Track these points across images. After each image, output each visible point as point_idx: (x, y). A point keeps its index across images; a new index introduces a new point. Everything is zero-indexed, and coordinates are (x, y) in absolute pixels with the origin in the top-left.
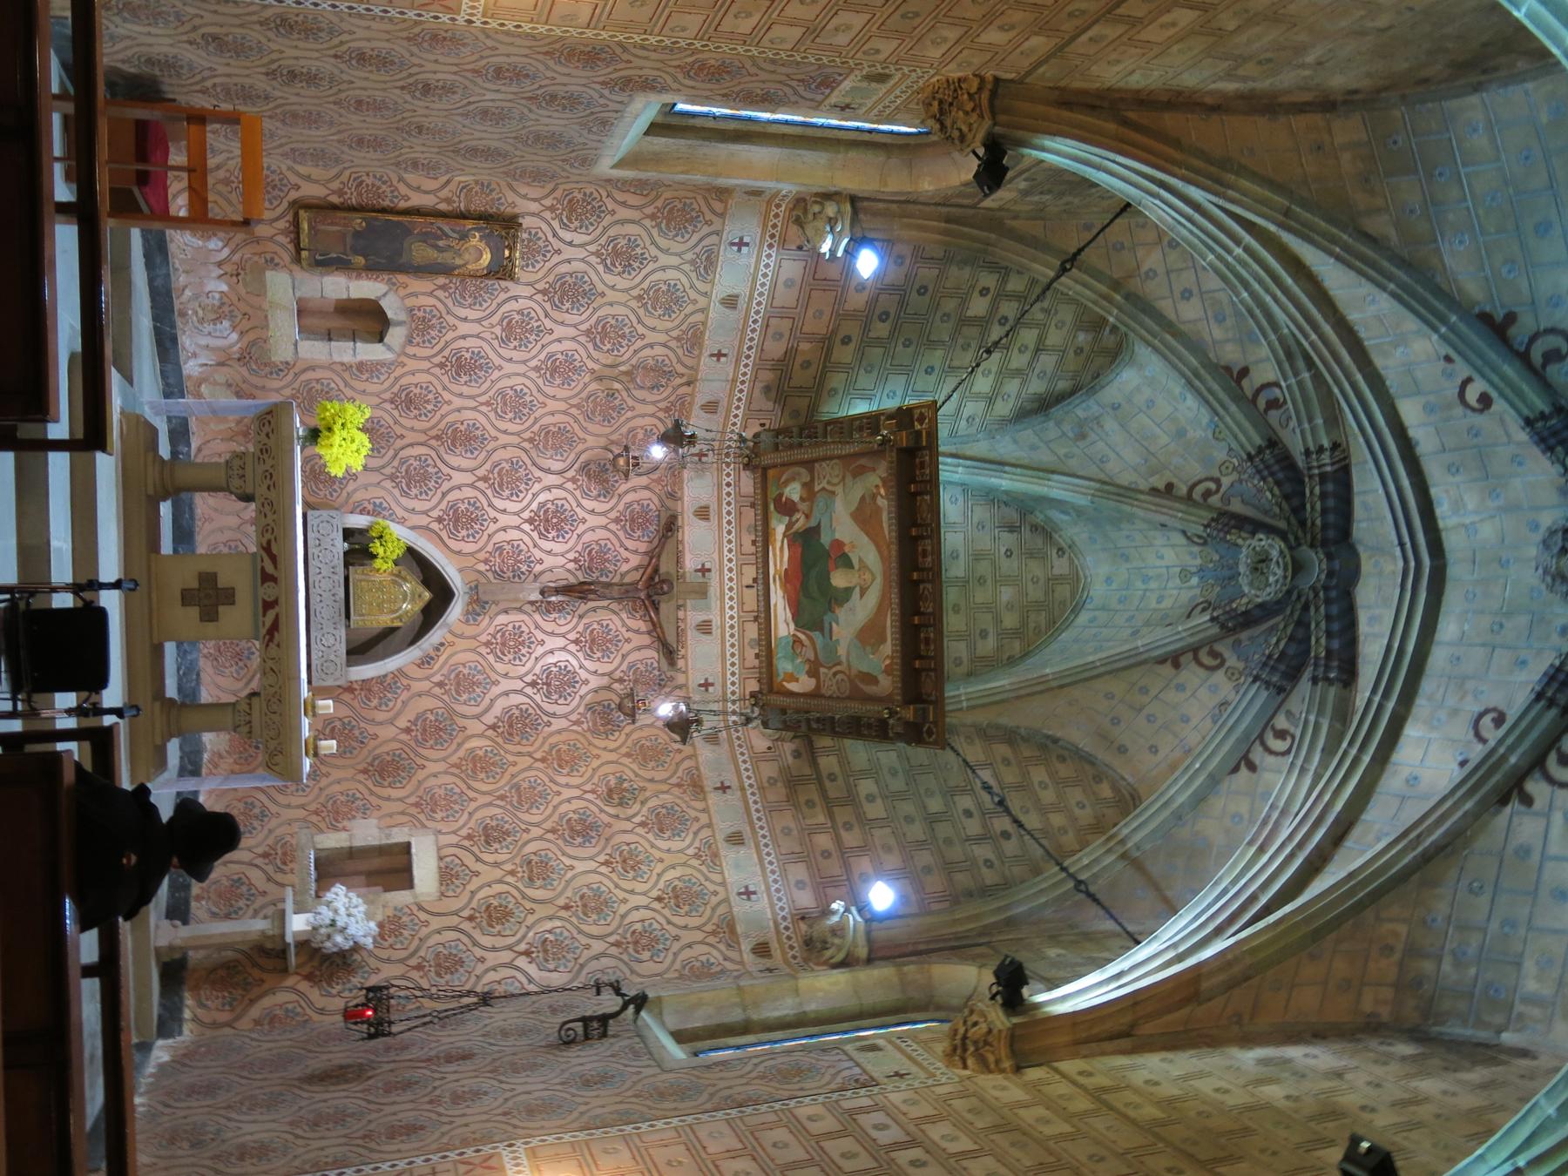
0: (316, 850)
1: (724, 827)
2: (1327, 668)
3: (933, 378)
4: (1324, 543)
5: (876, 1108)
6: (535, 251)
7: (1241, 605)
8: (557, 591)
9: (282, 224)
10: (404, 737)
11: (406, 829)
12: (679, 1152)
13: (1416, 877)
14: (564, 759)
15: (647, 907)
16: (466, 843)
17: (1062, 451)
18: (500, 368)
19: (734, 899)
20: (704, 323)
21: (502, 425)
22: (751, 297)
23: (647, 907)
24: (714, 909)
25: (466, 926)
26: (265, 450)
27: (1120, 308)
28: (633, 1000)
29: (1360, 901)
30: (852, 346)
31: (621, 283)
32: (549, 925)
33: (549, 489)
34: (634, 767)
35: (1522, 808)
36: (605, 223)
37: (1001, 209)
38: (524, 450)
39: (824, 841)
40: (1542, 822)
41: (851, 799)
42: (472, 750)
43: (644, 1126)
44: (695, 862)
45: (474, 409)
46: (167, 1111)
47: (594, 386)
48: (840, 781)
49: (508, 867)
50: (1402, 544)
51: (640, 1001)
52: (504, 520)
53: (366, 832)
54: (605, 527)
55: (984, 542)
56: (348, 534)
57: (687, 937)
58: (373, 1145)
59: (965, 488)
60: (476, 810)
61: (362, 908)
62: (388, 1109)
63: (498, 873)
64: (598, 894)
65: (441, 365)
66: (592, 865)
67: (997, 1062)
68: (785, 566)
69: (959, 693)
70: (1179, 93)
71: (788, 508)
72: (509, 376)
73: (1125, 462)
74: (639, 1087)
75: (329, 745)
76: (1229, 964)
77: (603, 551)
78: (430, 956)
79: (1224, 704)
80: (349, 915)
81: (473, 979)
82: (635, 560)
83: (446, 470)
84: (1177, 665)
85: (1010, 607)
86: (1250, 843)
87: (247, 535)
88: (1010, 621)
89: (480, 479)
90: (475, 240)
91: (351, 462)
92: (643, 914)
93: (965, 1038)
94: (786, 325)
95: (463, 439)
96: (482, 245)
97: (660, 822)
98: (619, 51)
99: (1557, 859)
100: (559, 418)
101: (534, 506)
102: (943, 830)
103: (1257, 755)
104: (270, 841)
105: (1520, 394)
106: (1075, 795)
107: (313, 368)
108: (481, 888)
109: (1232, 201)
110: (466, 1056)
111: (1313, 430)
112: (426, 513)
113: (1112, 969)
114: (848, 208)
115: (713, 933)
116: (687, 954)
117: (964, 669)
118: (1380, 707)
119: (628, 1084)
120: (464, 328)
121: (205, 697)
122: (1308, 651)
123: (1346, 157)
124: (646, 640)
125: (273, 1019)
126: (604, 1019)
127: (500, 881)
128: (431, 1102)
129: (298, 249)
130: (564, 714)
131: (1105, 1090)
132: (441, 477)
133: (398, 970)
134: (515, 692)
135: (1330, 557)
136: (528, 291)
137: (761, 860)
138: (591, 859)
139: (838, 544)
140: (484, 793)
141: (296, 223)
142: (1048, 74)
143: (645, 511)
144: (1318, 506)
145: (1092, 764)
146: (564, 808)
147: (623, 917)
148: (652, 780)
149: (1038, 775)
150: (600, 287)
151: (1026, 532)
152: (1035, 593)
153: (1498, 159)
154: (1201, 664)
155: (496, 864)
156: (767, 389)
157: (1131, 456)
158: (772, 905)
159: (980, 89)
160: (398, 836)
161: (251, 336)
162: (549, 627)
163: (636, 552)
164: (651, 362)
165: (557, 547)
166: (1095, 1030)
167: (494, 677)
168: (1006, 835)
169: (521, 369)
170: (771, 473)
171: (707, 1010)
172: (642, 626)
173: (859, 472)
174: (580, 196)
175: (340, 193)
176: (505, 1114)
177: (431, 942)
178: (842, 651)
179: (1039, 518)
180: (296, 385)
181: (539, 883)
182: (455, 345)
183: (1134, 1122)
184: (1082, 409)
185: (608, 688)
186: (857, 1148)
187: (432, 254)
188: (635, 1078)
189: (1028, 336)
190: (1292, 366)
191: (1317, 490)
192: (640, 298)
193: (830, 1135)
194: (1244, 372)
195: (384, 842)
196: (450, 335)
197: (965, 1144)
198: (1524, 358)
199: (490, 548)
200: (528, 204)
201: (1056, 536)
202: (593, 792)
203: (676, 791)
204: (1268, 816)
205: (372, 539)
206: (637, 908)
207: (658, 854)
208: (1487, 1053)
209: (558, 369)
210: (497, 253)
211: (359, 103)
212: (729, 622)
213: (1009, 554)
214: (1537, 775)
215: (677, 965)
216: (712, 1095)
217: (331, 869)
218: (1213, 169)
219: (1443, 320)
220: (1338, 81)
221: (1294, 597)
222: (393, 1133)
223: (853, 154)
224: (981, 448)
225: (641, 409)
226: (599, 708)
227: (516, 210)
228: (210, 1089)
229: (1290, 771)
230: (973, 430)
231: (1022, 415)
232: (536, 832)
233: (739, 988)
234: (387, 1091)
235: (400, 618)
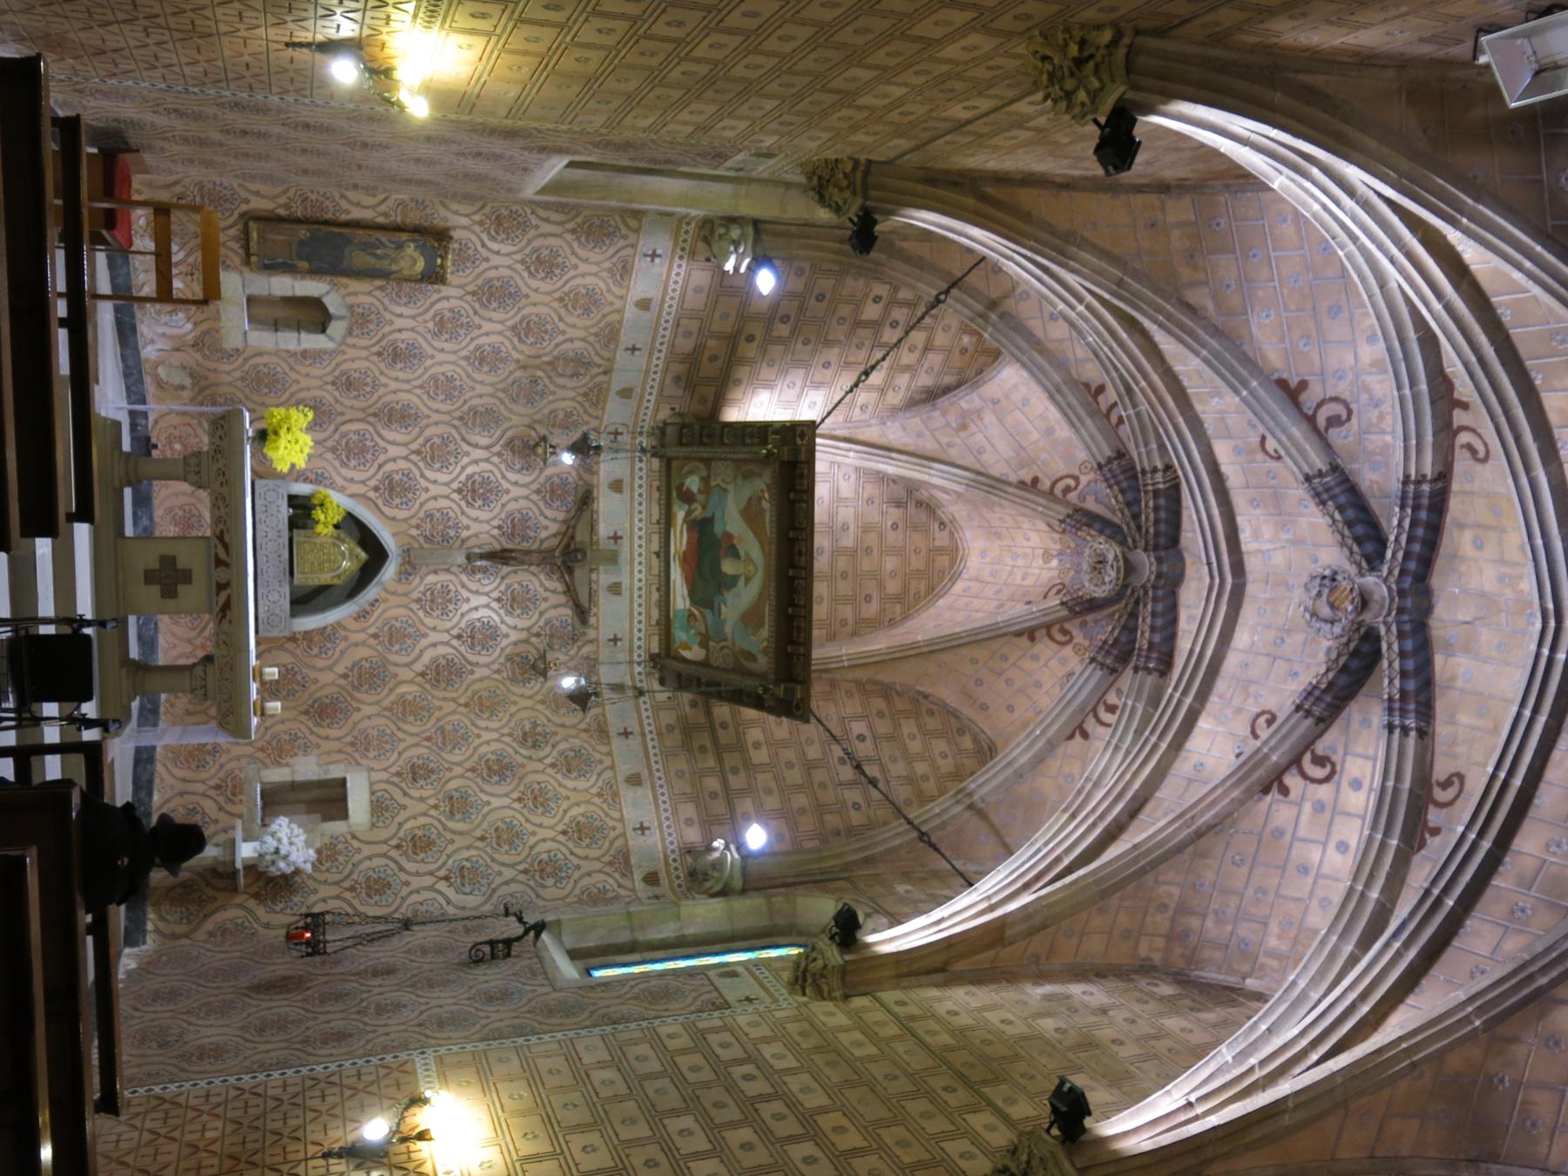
0: (263, 784)
1: (624, 769)
2: (1148, 658)
3: (829, 372)
4: (1156, 548)
5: (725, 1028)
6: (465, 259)
8: (482, 557)
9: (233, 232)
10: (342, 682)
11: (342, 766)
12: (559, 1062)
13: (1191, 849)
14: (485, 705)
15: (553, 840)
16: (396, 780)
17: (944, 440)
18: (432, 357)
20: (620, 322)
22: (663, 301)
23: (553, 840)
24: (611, 843)
26: (218, 451)
27: (994, 326)
28: (532, 928)
29: (1143, 868)
32: (466, 854)
33: (476, 462)
34: (548, 713)
35: (1281, 797)
37: (891, 232)
38: (455, 427)
39: (712, 783)
40: (1295, 810)
42: (403, 695)
43: (534, 1039)
44: (597, 800)
45: (409, 391)
46: (137, 1014)
47: (518, 374)
48: (731, 729)
49: (432, 802)
50: (1209, 564)
51: (539, 928)
52: (435, 490)
53: (306, 768)
54: (527, 498)
55: (874, 516)
56: (293, 500)
57: (587, 866)
58: (310, 1049)
60: (405, 750)
61: (303, 838)
62: (322, 1018)
63: (423, 807)
64: (510, 826)
65: (379, 354)
66: (507, 801)
68: (684, 547)
70: (1031, 174)
71: (688, 498)
72: (441, 364)
73: (999, 458)
74: (533, 1004)
75: (275, 706)
77: (525, 519)
78: (362, 880)
79: (1071, 674)
80: (291, 844)
82: (554, 528)
83: (382, 444)
84: (1032, 638)
85: (893, 574)
86: (1064, 811)
87: (200, 501)
88: (893, 587)
89: (413, 452)
90: (410, 250)
91: (295, 460)
93: (805, 971)
94: (694, 325)
95: (398, 416)
96: (416, 254)
97: (568, 764)
99: (1303, 840)
100: (485, 400)
101: (463, 478)
103: (1090, 725)
104: (222, 774)
105: (1302, 453)
106: (940, 746)
107: (260, 354)
108: (407, 820)
110: (389, 971)
111: (1149, 453)
112: (363, 482)
114: (750, 230)
115: (610, 863)
116: (586, 881)
117: (849, 628)
120: (400, 323)
121: (162, 659)
123: (1176, 234)
124: (562, 599)
125: (224, 932)
126: (508, 943)
127: (425, 814)
128: (359, 1012)
129: (248, 255)
130: (485, 664)
131: (912, 1018)
132: (376, 450)
134: (442, 643)
135: (1159, 560)
136: (459, 292)
137: (655, 797)
138: (506, 795)
139: (728, 536)
140: (412, 735)
141: (246, 233)
142: (914, 159)
143: (564, 482)
144: (1152, 517)
145: (957, 717)
146: (484, 749)
147: (532, 848)
148: (563, 725)
149: (908, 727)
150: (525, 290)
151: (911, 508)
152: (917, 563)
153: (1302, 248)
154: (1052, 639)
155: (422, 799)
156: (677, 379)
157: (1005, 449)
158: (663, 839)
159: (854, 169)
160: (335, 772)
161: (204, 327)
162: (474, 587)
163: (554, 520)
164: (571, 354)
165: (484, 515)
166: (915, 967)
167: (423, 629)
169: (453, 358)
170: (675, 464)
171: (604, 927)
172: (559, 587)
173: (748, 476)
174: (506, 213)
175: (287, 206)
176: (420, 1025)
178: (728, 629)
180: (246, 368)
181: (458, 816)
182: (392, 337)
183: (927, 1047)
184: (967, 401)
185: (526, 641)
186: (703, 1063)
187: (371, 261)
188: (530, 996)
189: (918, 337)
190: (1131, 399)
191: (1151, 504)
192: (561, 300)
194: (1101, 389)
195: (323, 777)
196: (387, 329)
197: (791, 1062)
198: (1311, 420)
199: (421, 515)
200: (460, 221)
201: (939, 512)
202: (510, 735)
203: (583, 735)
204: (1083, 787)
205: (313, 507)
206: (544, 840)
209: (484, 358)
210: (430, 262)
212: (637, 585)
213: (895, 526)
214: (1294, 770)
215: (577, 891)
216: (592, 1013)
217: (277, 800)
218: (1057, 242)
219: (1245, 384)
220: (1169, 174)
224: (872, 434)
225: (561, 393)
226: (517, 659)
227: (449, 224)
228: (173, 995)
229: (1105, 749)
230: (864, 417)
232: (458, 770)
233: (629, 914)
234: (322, 1002)
235: (339, 576)
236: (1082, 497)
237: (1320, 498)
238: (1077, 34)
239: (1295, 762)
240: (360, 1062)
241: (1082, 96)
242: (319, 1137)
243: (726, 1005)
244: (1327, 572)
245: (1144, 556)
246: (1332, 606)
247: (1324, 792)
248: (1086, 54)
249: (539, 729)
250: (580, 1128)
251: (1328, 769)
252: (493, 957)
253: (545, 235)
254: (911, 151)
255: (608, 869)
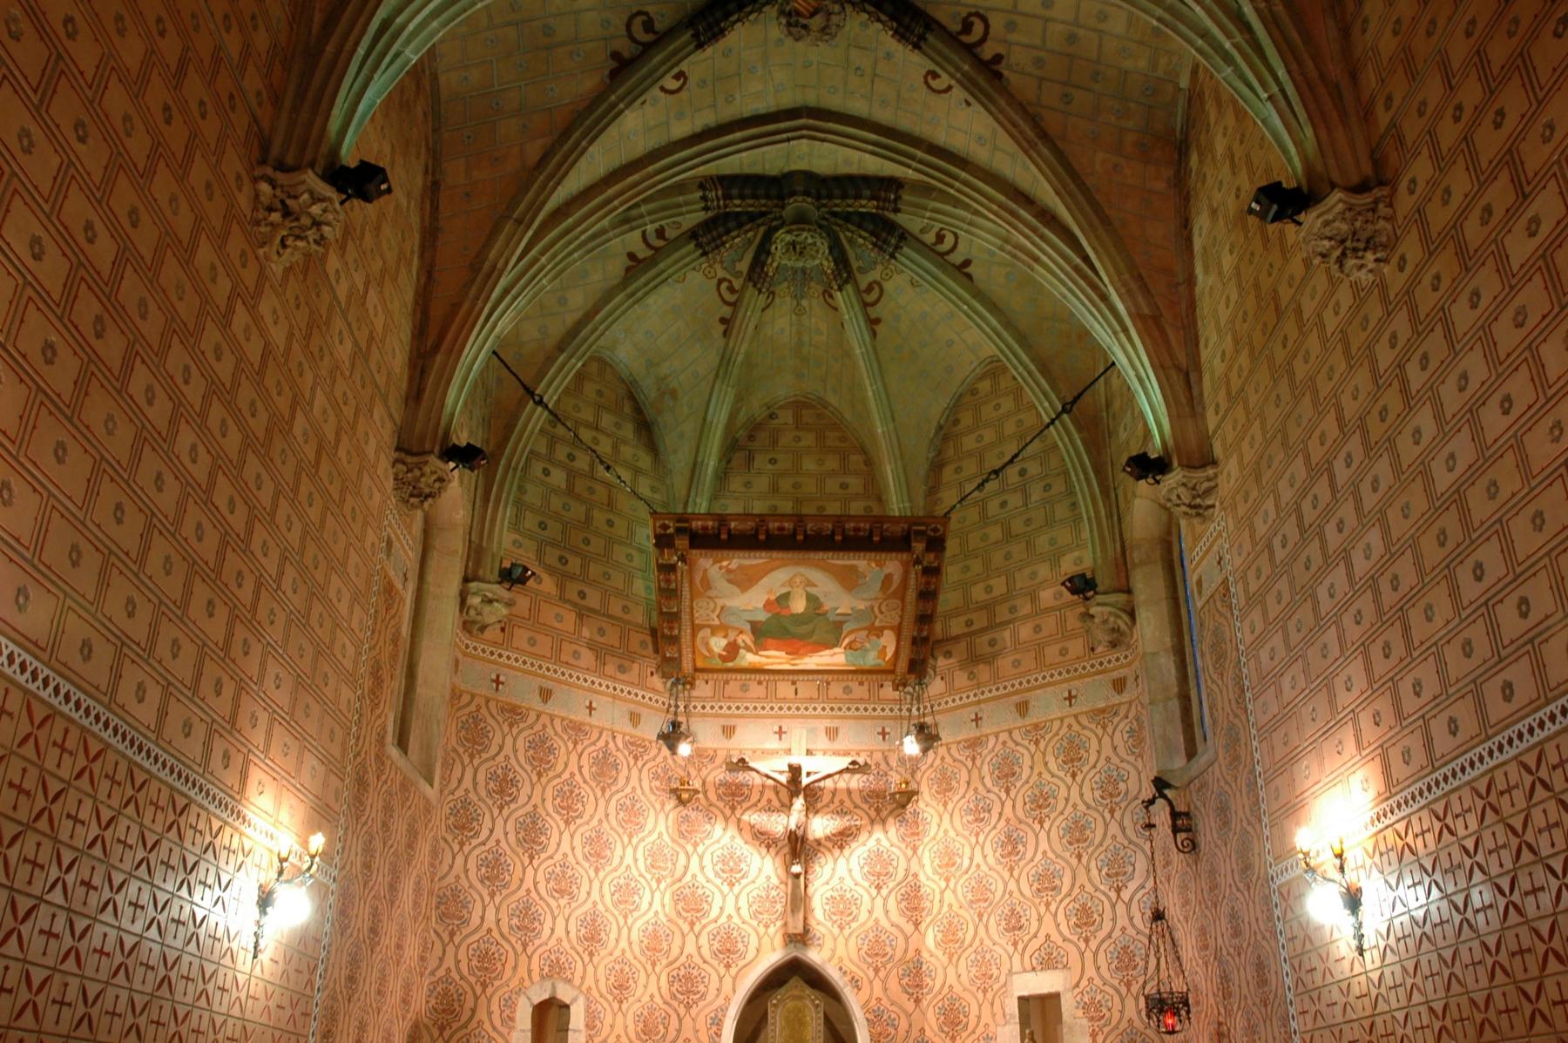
2: (886, 200)
4: (781, 198)
5: (1244, 578)
7: (829, 266)
13: (1059, 144)
18: (595, 904)
19: (1076, 709)
21: (645, 906)
25: (1093, 944)
30: (587, 590)
31: (526, 790)
32: (1094, 872)
33: (702, 868)
34: (956, 798)
36: (475, 799)
41: (989, 607)
42: (937, 944)
43: (1259, 769)
44: (1042, 744)
49: (1042, 909)
50: (789, 140)
51: (1160, 784)
52: (730, 909)
57: (1107, 751)
58: (1271, 997)
59: (715, 497)
63: (1048, 918)
64: (1069, 830)
66: (1043, 835)
67: (1209, 479)
68: (782, 654)
69: (896, 505)
70: (416, 302)
71: (733, 650)
76: (1129, 291)
81: (1140, 937)
83: (683, 959)
84: (877, 321)
88: (832, 463)
92: (1086, 790)
93: (1190, 506)
97: (1006, 776)
98: (359, 760)
99: (1044, 41)
101: (719, 882)
102: (1018, 526)
103: (957, 258)
106: (988, 412)
108: (1061, 933)
109: (507, 263)
111: (687, 204)
113: (1136, 385)
114: (473, 585)
116: (1121, 751)
118: (921, 162)
119: (1227, 788)
122: (870, 214)
126: (1175, 815)
127: (1055, 916)
131: (1229, 393)
133: (1130, 1002)
134: (885, 905)
135: (793, 194)
144: (750, 201)
145: (961, 396)
146: (991, 860)
147: (1089, 807)
149: (969, 443)
150: (529, 808)
152: (808, 439)
154: (877, 301)
156: (622, 669)
159: (404, 463)
160: (1013, 1008)
166: (1184, 400)
167: (871, 923)
168: (1022, 473)
170: (700, 664)
173: (706, 583)
177: (1106, 975)
178: (862, 606)
179: (741, 434)
181: (1057, 882)
183: (1251, 371)
189: (586, 435)
191: (737, 202)
193: (1265, 613)
194: (632, 256)
198: (647, 49)
199: (755, 923)
202: (977, 835)
206: (1081, 795)
207: (1035, 777)
208: (1195, 97)
211: (379, 992)
213: (773, 461)
214: (978, 50)
215: (1131, 759)
216: (1236, 716)
218: (479, 279)
221: (824, 223)
222: (1263, 982)
223: (430, 578)
231: (653, 447)
236: (737, 274)
237: (716, 33)
238: (261, 214)
239: (970, 49)
240: (1282, 940)
241: (316, 210)
242: (1346, 964)
243: (1225, 581)
244: (784, 21)
245: (789, 208)
246: (812, 15)
247: (997, 23)
248: (279, 206)
249: (972, 806)
250: (1332, 701)
251: (973, 19)
252: (1188, 830)
253: (475, 784)
254: (387, 407)
255: (1110, 730)
